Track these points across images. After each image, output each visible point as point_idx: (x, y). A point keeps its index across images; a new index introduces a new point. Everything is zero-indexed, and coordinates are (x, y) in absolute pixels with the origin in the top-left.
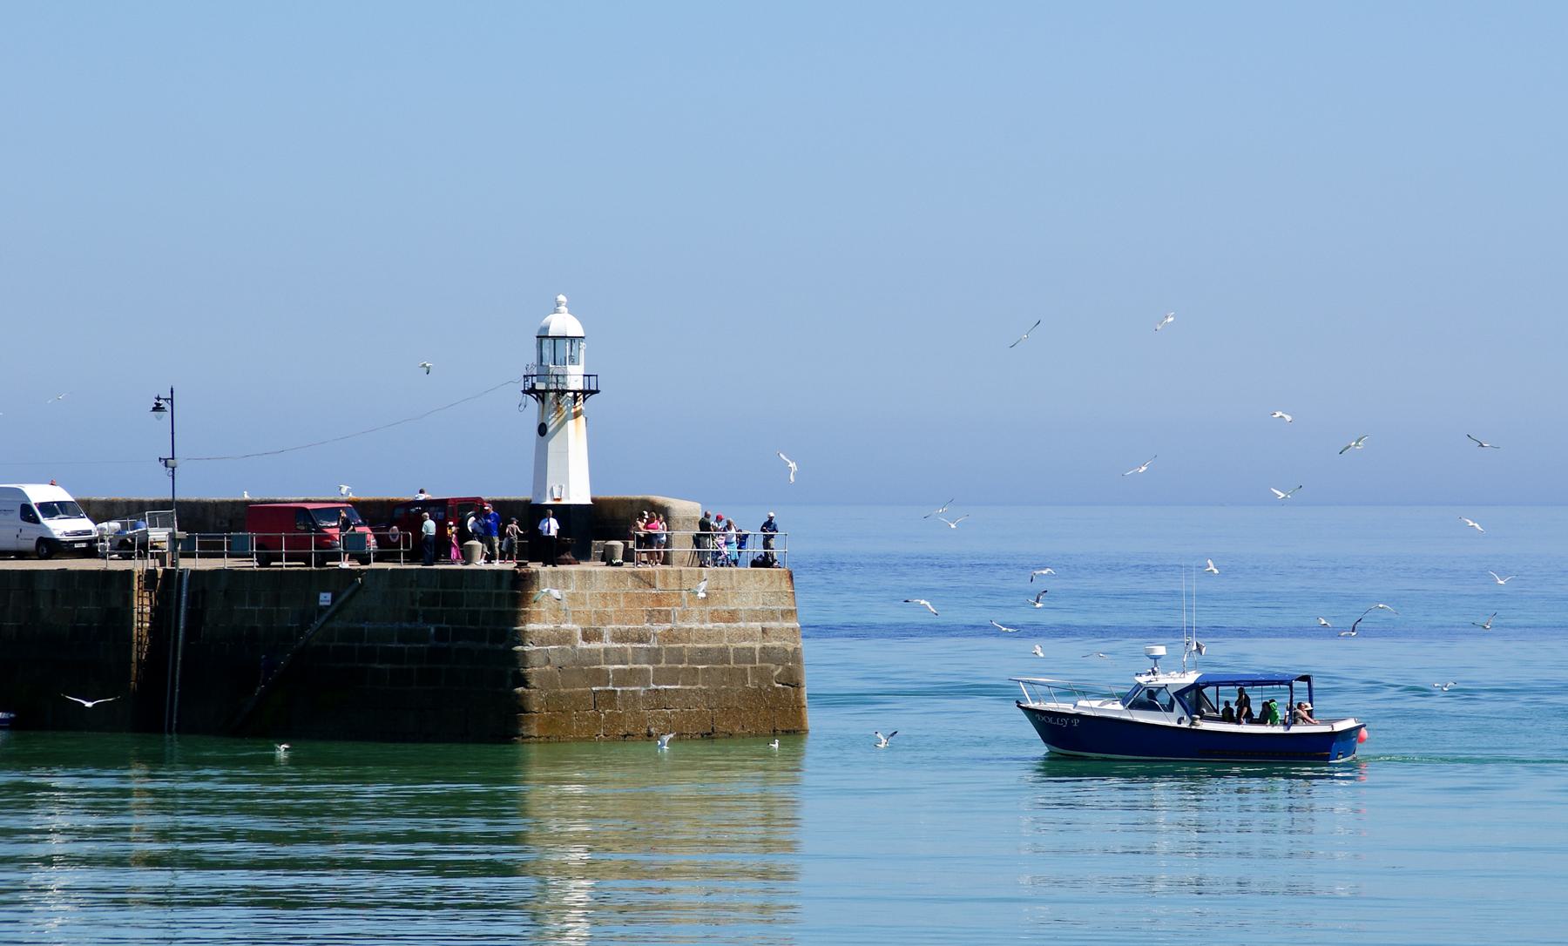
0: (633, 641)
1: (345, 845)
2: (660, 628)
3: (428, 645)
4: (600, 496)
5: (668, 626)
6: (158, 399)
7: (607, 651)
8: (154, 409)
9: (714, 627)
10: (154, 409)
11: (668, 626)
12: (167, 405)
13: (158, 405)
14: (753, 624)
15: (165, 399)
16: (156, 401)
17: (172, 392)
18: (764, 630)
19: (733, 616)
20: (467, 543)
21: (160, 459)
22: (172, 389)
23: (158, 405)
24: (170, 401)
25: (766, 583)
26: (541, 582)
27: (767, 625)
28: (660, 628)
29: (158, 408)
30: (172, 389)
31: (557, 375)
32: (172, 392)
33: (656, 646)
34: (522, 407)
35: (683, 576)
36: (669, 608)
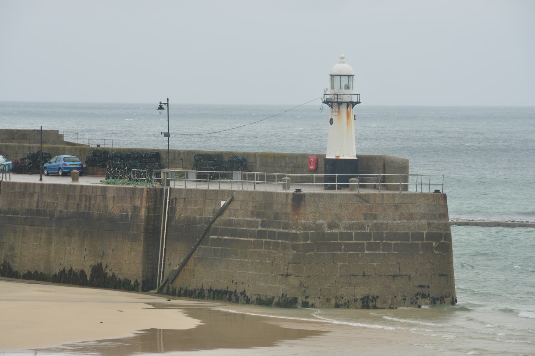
0: (356, 229)
1: (330, 320)
2: (371, 223)
3: (257, 229)
4: (361, 153)
5: (375, 222)
6: (161, 103)
7: (341, 234)
8: (159, 109)
9: (401, 222)
10: (159, 109)
11: (375, 222)
12: (164, 106)
13: (161, 106)
14: (423, 221)
15: (164, 103)
16: (160, 104)
17: (168, 100)
18: (429, 224)
19: (411, 217)
20: (283, 179)
21: (162, 133)
22: (168, 98)
23: (161, 106)
24: (167, 105)
25: (431, 201)
26: (307, 199)
27: (431, 221)
28: (371, 223)
29: (161, 108)
30: (168, 98)
31: (338, 95)
32: (168, 100)
33: (368, 231)
34: (321, 110)
35: (384, 197)
36: (377, 213)
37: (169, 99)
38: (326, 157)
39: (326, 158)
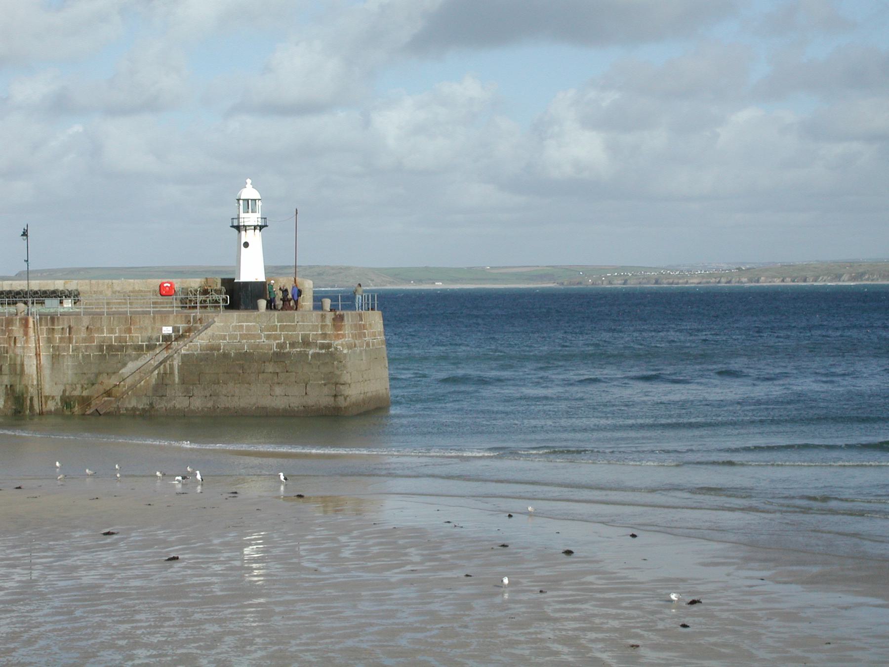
30: (297, 210)
37: (298, 212)
38: (234, 279)
39: (235, 281)
